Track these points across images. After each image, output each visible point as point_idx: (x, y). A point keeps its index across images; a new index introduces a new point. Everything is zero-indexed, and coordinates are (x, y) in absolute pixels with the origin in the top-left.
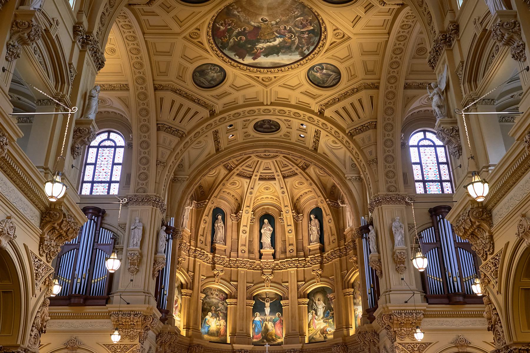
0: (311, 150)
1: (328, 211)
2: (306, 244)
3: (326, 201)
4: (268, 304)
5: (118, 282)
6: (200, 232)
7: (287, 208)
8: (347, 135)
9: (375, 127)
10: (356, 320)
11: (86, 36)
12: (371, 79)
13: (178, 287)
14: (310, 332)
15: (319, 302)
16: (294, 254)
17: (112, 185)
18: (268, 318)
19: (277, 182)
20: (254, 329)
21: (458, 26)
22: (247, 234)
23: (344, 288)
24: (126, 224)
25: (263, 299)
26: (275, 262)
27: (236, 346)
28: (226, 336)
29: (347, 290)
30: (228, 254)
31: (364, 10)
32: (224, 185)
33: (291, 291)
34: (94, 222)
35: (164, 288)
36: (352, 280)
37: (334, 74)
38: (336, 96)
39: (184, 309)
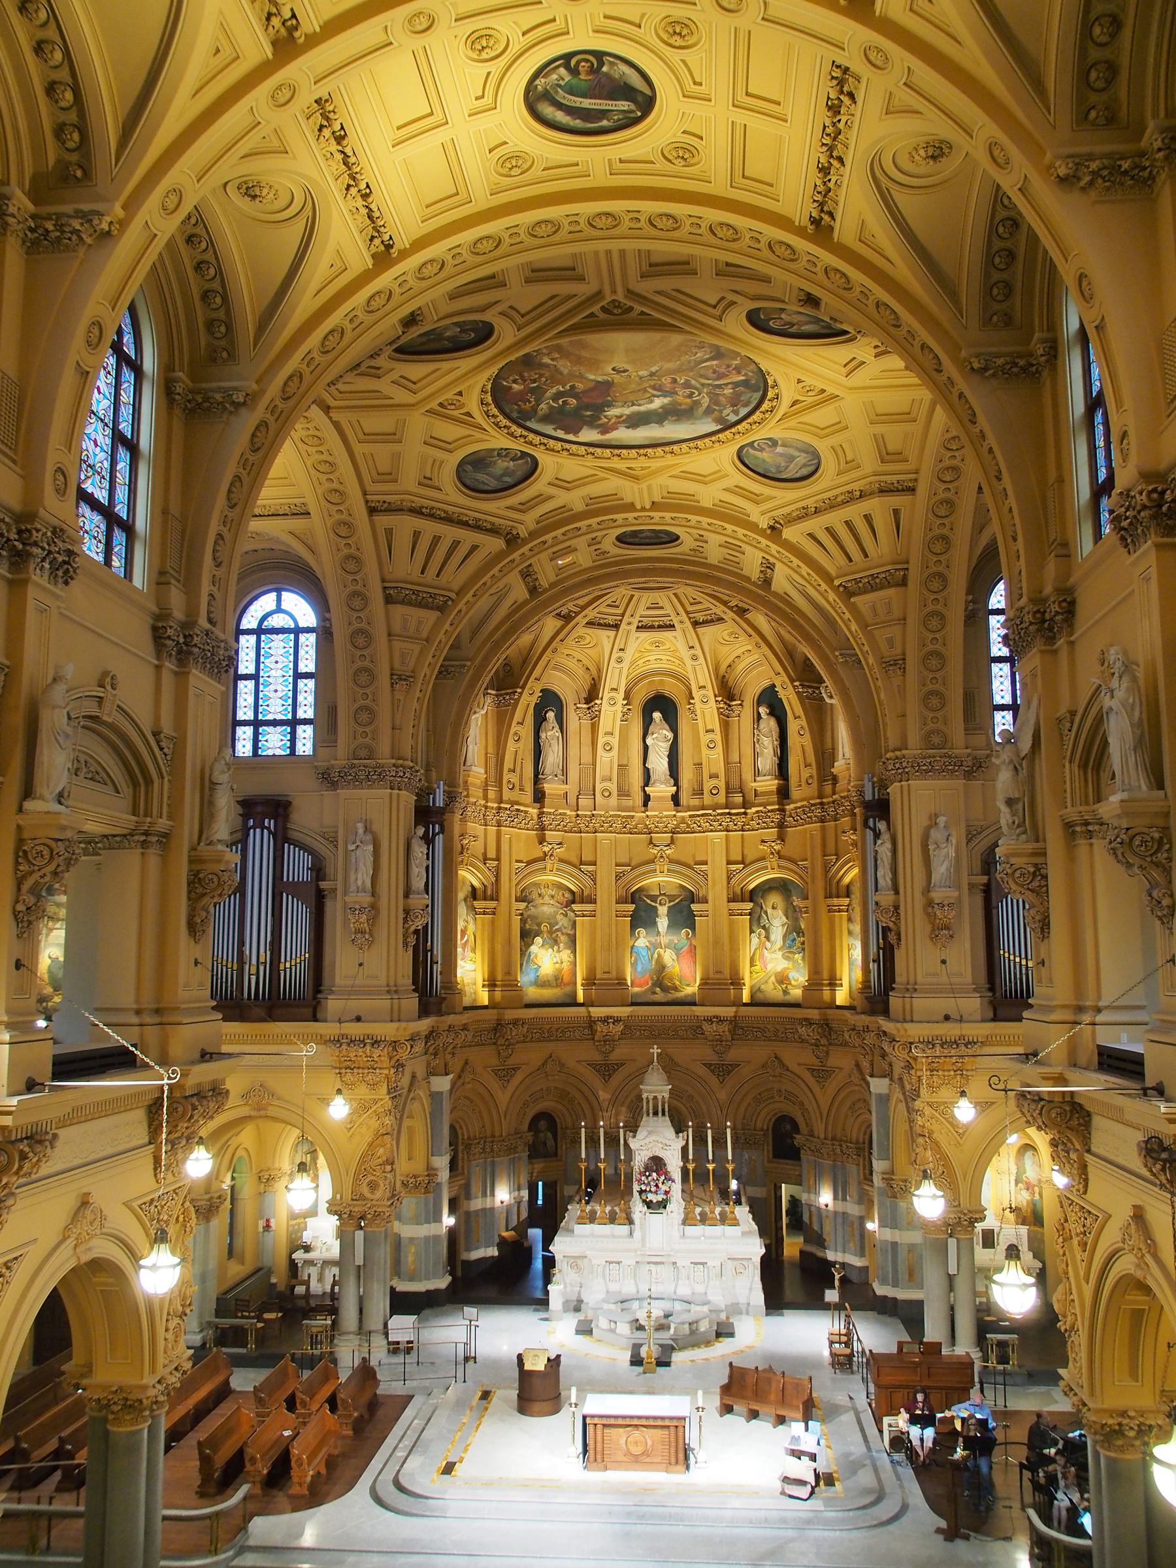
0: (754, 584)
1: (799, 711)
2: (748, 775)
3: (794, 687)
4: (663, 910)
5: (333, 963)
6: (508, 764)
7: (703, 692)
8: (835, 589)
9: (903, 583)
10: (850, 970)
11: (185, 636)
12: (895, 474)
13: (465, 900)
14: (755, 976)
15: (774, 912)
16: (721, 798)
17: (300, 729)
18: (664, 940)
19: (678, 633)
20: (634, 965)
21: (1073, 603)
22: (615, 753)
23: (829, 896)
24: (337, 827)
25: (654, 898)
26: (679, 814)
27: (597, 1012)
28: (575, 984)
29: (835, 901)
30: (572, 799)
31: (681, 1468)
32: (555, 651)
33: (714, 885)
34: (270, 832)
35: (432, 950)
36: (847, 880)
37: (804, 455)
38: (811, 503)
39: (483, 940)
